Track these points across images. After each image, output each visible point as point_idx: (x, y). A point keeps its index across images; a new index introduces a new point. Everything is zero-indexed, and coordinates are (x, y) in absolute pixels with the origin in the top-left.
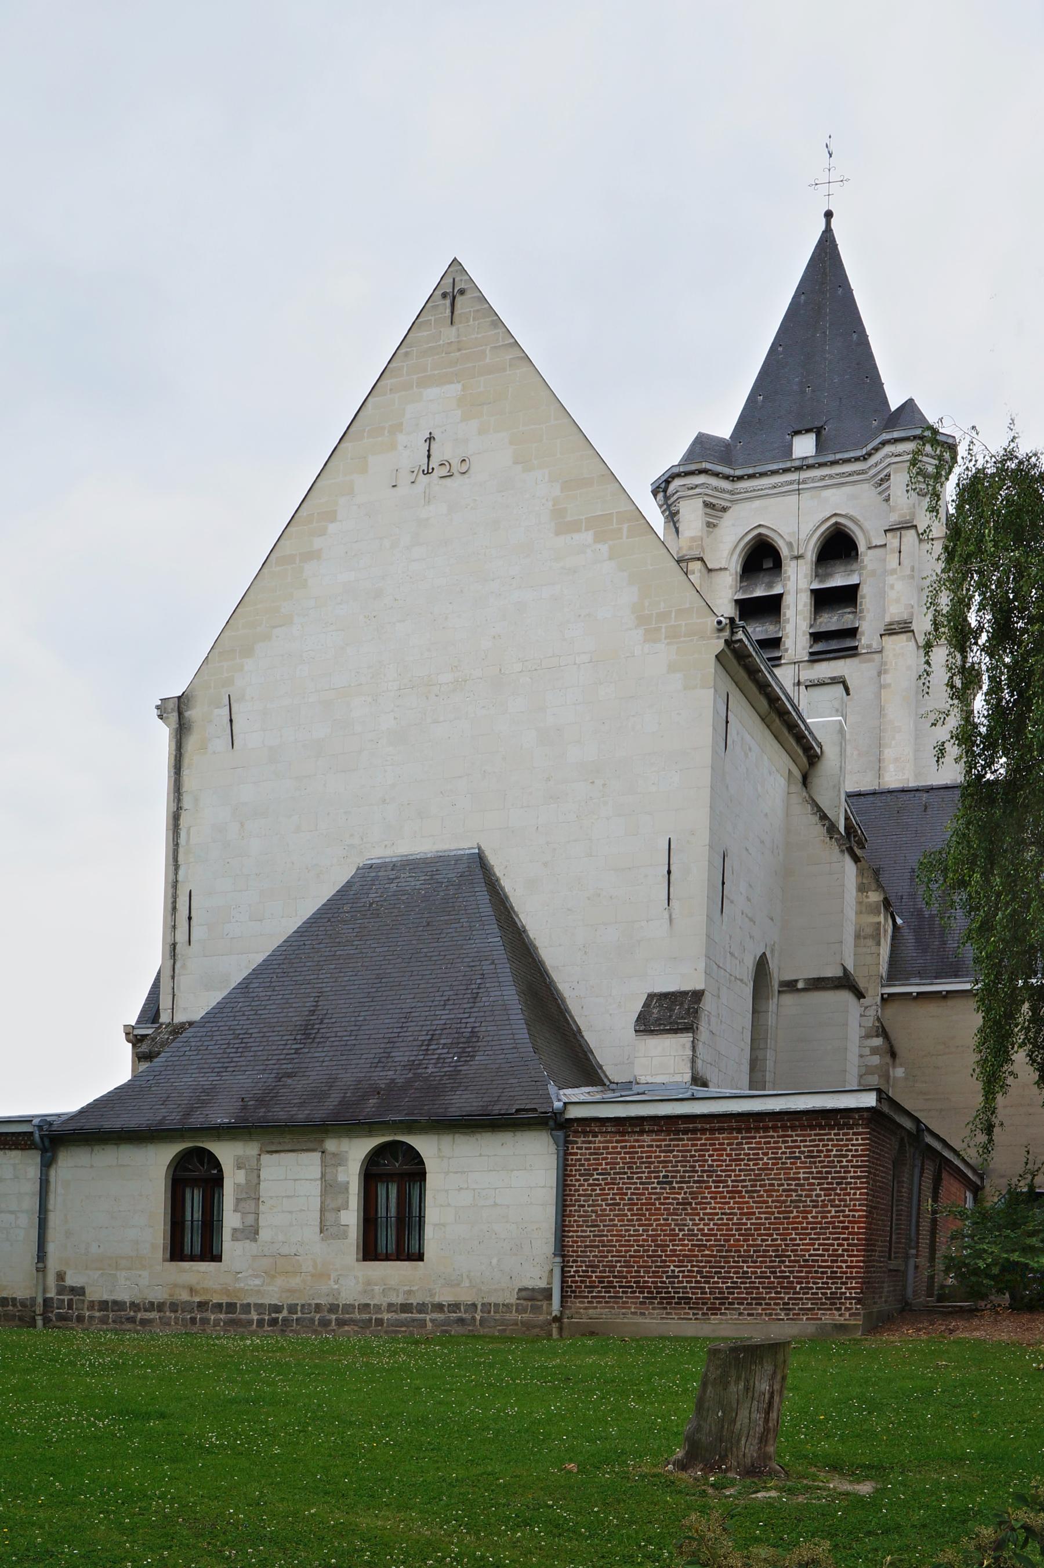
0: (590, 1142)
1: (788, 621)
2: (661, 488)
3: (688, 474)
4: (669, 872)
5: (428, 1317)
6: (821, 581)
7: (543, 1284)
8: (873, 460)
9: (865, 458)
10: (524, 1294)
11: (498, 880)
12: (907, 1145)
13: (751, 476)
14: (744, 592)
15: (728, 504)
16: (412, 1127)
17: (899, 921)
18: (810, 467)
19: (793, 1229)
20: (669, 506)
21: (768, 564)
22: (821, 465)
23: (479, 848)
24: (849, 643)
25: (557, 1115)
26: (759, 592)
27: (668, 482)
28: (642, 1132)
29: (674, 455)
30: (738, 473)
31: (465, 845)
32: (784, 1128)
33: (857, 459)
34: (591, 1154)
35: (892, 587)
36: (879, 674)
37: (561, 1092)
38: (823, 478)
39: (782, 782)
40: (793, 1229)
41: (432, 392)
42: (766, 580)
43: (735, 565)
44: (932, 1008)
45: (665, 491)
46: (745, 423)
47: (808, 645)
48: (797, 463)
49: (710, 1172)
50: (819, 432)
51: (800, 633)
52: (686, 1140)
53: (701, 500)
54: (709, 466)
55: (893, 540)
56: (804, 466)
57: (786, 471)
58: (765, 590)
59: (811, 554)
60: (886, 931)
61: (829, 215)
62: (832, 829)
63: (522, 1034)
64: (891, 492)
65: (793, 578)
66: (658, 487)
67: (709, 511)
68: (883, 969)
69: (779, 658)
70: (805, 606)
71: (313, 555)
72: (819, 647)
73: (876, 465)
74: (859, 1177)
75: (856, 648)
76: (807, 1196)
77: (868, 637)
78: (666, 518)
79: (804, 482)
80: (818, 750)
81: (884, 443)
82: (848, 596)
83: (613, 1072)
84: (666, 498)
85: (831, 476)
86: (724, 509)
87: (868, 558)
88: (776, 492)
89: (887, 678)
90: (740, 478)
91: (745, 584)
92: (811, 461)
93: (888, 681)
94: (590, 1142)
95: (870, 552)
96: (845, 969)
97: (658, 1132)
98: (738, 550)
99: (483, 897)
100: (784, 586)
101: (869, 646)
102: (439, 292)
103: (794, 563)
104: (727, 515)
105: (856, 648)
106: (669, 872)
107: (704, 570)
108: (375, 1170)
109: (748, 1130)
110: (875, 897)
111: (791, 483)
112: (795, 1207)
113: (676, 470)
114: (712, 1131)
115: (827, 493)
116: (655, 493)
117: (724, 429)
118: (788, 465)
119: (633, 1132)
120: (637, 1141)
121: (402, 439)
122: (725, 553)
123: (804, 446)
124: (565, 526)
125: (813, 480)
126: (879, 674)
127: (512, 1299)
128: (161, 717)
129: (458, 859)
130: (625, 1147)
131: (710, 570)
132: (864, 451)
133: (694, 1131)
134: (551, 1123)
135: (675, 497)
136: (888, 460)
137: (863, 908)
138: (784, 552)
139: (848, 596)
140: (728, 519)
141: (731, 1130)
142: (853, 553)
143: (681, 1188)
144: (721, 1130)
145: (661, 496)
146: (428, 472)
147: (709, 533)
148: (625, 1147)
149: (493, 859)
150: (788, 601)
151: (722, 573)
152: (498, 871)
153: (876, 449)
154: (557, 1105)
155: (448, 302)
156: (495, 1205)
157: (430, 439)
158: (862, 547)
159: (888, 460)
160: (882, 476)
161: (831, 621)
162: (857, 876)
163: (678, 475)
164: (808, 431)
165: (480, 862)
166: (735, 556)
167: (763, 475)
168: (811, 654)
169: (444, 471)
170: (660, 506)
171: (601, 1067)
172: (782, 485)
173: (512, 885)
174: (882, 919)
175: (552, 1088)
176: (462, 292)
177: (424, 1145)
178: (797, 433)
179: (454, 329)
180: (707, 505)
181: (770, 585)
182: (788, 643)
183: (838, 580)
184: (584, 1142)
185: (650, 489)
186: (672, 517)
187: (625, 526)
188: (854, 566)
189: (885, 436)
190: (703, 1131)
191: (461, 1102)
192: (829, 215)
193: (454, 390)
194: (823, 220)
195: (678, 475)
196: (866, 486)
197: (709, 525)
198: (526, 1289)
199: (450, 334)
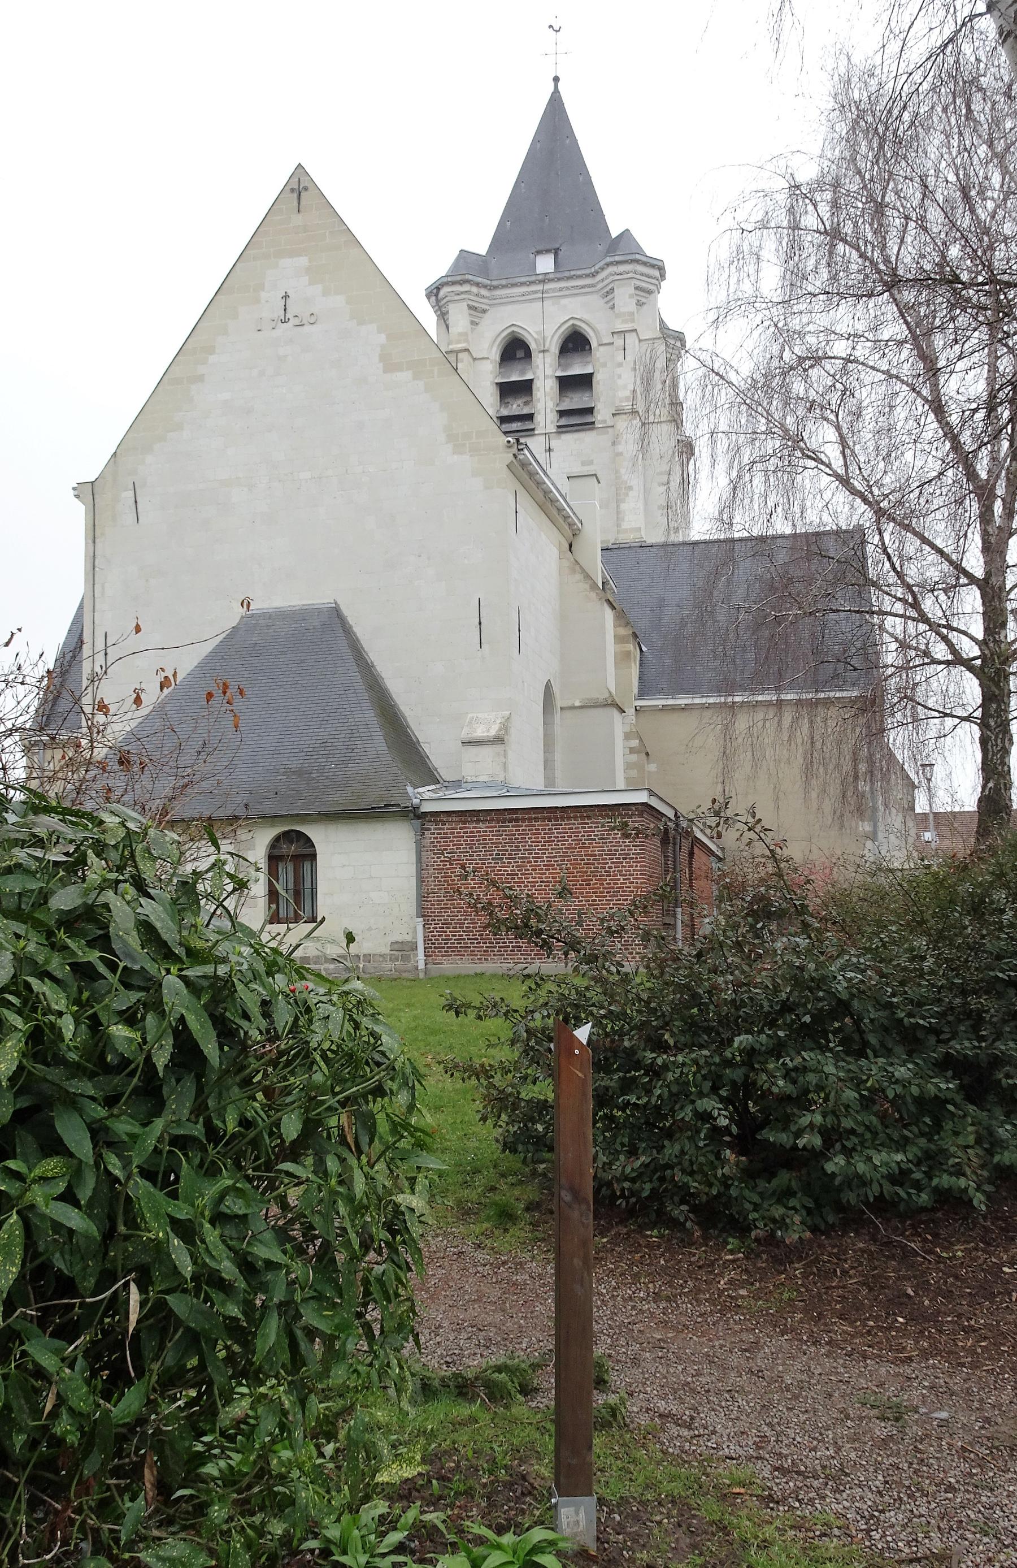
0: (440, 829)
1: (538, 401)
2: (434, 292)
3: (454, 283)
4: (480, 623)
5: (322, 967)
6: (563, 370)
7: (409, 938)
8: (599, 277)
9: (593, 275)
10: (396, 947)
11: (351, 627)
12: (137, 1077)
13: (504, 287)
14: (503, 377)
15: (487, 307)
16: (305, 818)
17: (644, 649)
18: (551, 280)
19: (594, 893)
20: (440, 308)
21: (520, 354)
22: (559, 279)
23: (336, 603)
24: (589, 419)
25: (416, 808)
26: (515, 378)
27: (438, 289)
28: (478, 821)
29: (441, 267)
30: (494, 283)
31: (320, 597)
32: (582, 817)
33: (587, 276)
34: (442, 838)
35: (620, 377)
36: (614, 444)
37: (416, 791)
38: (561, 289)
39: (555, 552)
40: (594, 893)
41: (286, 262)
42: (520, 367)
43: (495, 354)
44: (675, 717)
45: (436, 296)
46: (498, 242)
47: (556, 420)
48: (541, 277)
49: (530, 851)
50: (556, 252)
51: (548, 410)
52: (511, 827)
53: (465, 304)
54: (470, 277)
55: (619, 342)
56: (545, 279)
57: (531, 283)
58: (520, 376)
59: (555, 349)
60: (635, 657)
61: (556, 79)
62: (594, 586)
63: (383, 747)
64: (616, 302)
65: (541, 367)
66: (431, 292)
67: (472, 312)
68: (635, 691)
69: (533, 430)
70: (552, 388)
71: (200, 379)
72: (564, 421)
73: (603, 280)
74: (638, 854)
75: (594, 423)
76: (602, 868)
77: (602, 415)
78: (438, 316)
79: (547, 292)
80: (580, 525)
81: (608, 265)
82: (585, 382)
83: (446, 773)
84: (438, 301)
85: (567, 288)
86: (484, 311)
87: (599, 353)
88: (525, 299)
89: (620, 448)
90: (496, 287)
91: (502, 370)
92: (551, 276)
93: (620, 450)
94: (440, 829)
95: (601, 348)
96: (610, 692)
97: (489, 821)
98: (499, 339)
99: (343, 643)
100: (534, 373)
101: (605, 421)
102: (288, 188)
103: (541, 355)
104: (487, 316)
105: (594, 423)
106: (480, 623)
107: (471, 360)
108: (276, 852)
109: (556, 819)
110: (623, 631)
111: (536, 292)
112: (594, 876)
113: (445, 280)
114: (530, 820)
115: (564, 301)
116: (428, 296)
117: (481, 246)
118: (533, 278)
119: (472, 821)
120: (475, 828)
121: (263, 295)
122: (486, 346)
123: (545, 264)
124: (390, 366)
125: (554, 290)
126: (614, 444)
127: (386, 950)
128: (77, 496)
129: (320, 611)
130: (466, 832)
131: (475, 359)
132: (593, 270)
133: (517, 820)
134: (411, 815)
135: (445, 301)
136: (611, 278)
137: (619, 639)
138: (533, 346)
139: (585, 382)
140: (486, 320)
141: (543, 819)
142: (587, 347)
143: (509, 863)
144: (536, 819)
145: (433, 298)
146: (285, 321)
147: (472, 330)
148: (466, 832)
149: (346, 611)
150: (537, 385)
151: (484, 362)
152: (351, 621)
153: (602, 269)
154: (416, 801)
155: (295, 195)
156: (371, 877)
157: (286, 297)
158: (594, 344)
159: (611, 278)
160: (608, 289)
161: (576, 400)
162: (615, 620)
163: (447, 284)
164: (548, 251)
165: (336, 613)
166: (495, 349)
167: (514, 285)
168: (559, 427)
169: (297, 322)
170: (433, 307)
171: (436, 769)
172: (529, 293)
173: (360, 631)
174: (632, 648)
175: (410, 789)
176: (306, 189)
177: (315, 833)
178: (539, 252)
179: (300, 216)
180: (470, 307)
181: (523, 373)
182: (539, 418)
183: (576, 370)
184: (436, 829)
185: (424, 293)
186: (442, 316)
187: (436, 369)
188: (588, 359)
189: (608, 259)
190: (523, 820)
191: (339, 799)
192: (556, 79)
193: (303, 261)
194: (552, 84)
195: (447, 284)
196: (595, 297)
197: (473, 323)
198: (397, 942)
199: (297, 220)
